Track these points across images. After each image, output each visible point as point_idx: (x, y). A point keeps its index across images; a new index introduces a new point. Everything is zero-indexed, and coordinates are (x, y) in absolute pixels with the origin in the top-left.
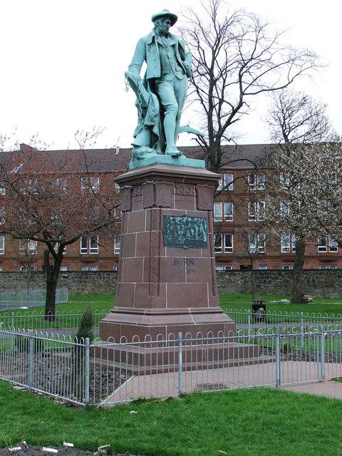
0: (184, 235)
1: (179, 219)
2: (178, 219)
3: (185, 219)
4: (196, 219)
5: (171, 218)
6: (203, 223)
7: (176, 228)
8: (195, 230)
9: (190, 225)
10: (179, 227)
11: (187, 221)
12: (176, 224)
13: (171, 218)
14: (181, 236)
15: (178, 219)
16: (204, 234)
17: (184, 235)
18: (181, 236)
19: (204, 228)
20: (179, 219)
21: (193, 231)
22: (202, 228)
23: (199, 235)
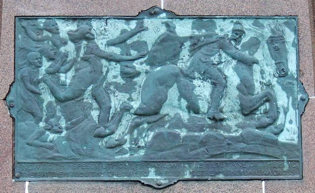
0: (151, 113)
1: (115, 29)
2: (107, 32)
3: (154, 30)
4: (225, 28)
5: (65, 28)
6: (276, 44)
7: (97, 76)
8: (219, 84)
9: (185, 60)
10: (114, 73)
11: (169, 45)
12: (94, 56)
13: (65, 28)
14: (127, 120)
15: (107, 32)
16: (282, 99)
17: (151, 113)
18: (127, 120)
19: (282, 73)
20: (115, 29)
21: (203, 90)
22: (265, 69)
23: (248, 111)
